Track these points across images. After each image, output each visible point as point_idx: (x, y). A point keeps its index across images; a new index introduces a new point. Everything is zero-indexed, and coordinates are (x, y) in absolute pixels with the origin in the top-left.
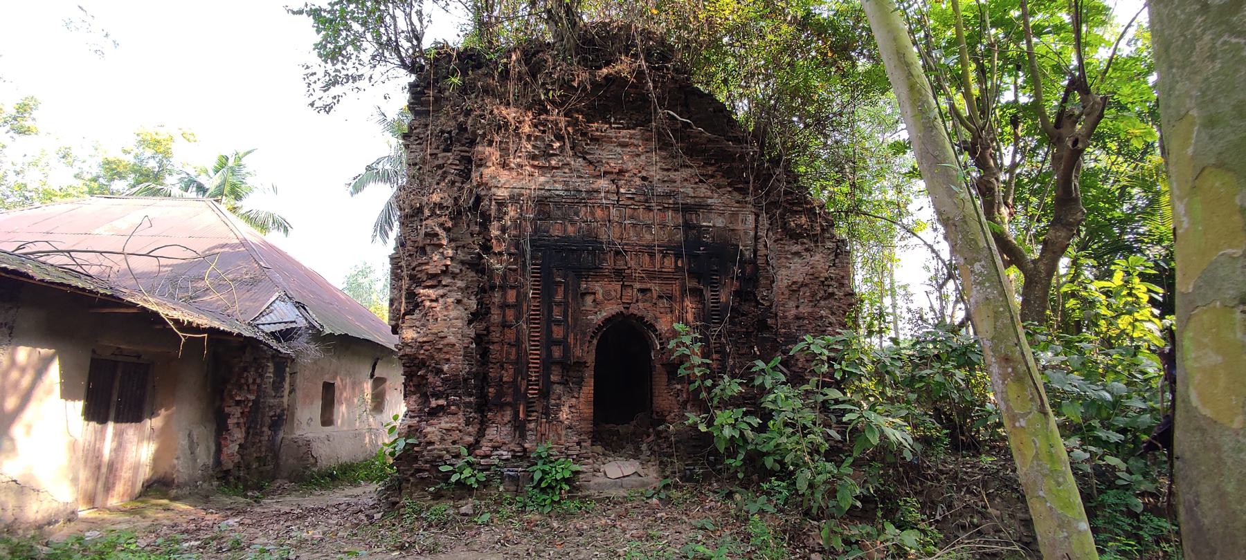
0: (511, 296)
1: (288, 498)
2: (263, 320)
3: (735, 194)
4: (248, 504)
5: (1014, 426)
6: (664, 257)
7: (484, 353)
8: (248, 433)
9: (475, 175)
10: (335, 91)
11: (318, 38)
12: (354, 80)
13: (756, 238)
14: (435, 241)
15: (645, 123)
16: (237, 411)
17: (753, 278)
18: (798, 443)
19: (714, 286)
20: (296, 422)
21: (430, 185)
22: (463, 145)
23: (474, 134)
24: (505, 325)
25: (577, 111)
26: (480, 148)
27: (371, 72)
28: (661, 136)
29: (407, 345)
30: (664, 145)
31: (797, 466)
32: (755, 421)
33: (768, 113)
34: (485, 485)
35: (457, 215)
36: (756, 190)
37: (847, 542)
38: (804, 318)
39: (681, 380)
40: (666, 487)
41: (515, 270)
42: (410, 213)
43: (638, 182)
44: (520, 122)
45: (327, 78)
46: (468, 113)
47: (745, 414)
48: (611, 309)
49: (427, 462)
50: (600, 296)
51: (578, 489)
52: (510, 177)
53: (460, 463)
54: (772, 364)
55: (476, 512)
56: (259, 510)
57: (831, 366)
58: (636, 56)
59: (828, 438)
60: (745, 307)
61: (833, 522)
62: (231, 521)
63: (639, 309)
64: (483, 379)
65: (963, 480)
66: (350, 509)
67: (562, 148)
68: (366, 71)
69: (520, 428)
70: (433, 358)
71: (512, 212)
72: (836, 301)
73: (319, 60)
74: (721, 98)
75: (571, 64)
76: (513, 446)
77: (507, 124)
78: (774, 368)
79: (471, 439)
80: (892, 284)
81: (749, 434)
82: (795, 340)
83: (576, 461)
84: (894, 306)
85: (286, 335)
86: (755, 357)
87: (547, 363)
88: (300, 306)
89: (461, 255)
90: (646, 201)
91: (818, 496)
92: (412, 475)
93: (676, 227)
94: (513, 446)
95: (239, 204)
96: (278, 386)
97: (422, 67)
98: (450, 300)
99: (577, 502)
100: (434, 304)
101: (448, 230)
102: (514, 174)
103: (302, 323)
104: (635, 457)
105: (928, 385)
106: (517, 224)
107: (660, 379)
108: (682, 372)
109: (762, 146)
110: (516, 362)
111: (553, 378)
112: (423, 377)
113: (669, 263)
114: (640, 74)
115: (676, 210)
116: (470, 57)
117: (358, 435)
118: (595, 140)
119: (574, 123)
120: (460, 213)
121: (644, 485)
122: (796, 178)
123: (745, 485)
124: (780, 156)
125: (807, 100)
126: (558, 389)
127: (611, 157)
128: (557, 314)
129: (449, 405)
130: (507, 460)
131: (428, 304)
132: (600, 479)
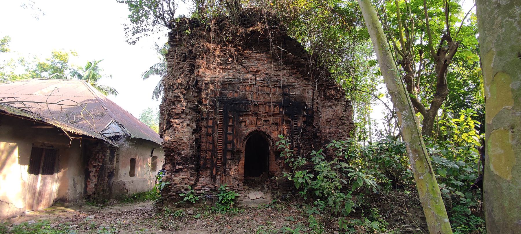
0: (211, 123)
1: (115, 207)
2: (105, 132)
3: (305, 81)
4: (98, 209)
5: (419, 179)
6: (275, 107)
7: (199, 147)
8: (98, 179)
9: (196, 72)
10: (137, 35)
11: (130, 13)
12: (145, 31)
13: (313, 99)
14: (179, 99)
15: (267, 51)
16: (94, 170)
17: (311, 116)
18: (329, 185)
19: (296, 119)
20: (119, 175)
21: (177, 75)
22: (191, 59)
23: (196, 54)
24: (208, 135)
25: (239, 46)
26: (198, 60)
27: (152, 28)
28: (274, 56)
29: (166, 143)
30: (275, 60)
31: (329, 195)
32: (312, 176)
33: (319, 48)
34: (199, 202)
35: (188, 88)
36: (313, 79)
37: (349, 226)
38: (332, 133)
39: (281, 158)
40: (274, 203)
41: (212, 112)
42: (168, 87)
43: (264, 75)
44: (215, 50)
45: (134, 30)
46: (193, 46)
47: (307, 173)
48: (252, 129)
49: (174, 192)
50: (248, 123)
51: (237, 204)
52: (210, 73)
53: (188, 192)
54: (319, 152)
55: (195, 213)
56: (103, 212)
57: (343, 153)
58: (264, 23)
59: (342, 183)
60: (308, 128)
61: (343, 218)
62: (91, 217)
63: (264, 128)
64: (198, 157)
65: (397, 201)
66: (142, 212)
67: (232, 61)
68: (150, 27)
69: (213, 178)
70: (177, 148)
71: (211, 87)
72: (346, 126)
73: (131, 23)
74: (299, 41)
75: (237, 26)
76: (210, 186)
77: (209, 50)
78: (320, 154)
79: (193, 183)
80: (369, 119)
81: (309, 181)
82: (329, 142)
83: (237, 192)
84: (370, 129)
85: (115, 138)
86: (312, 149)
87: (225, 151)
88: (121, 126)
89: (189, 105)
90: (267, 84)
91: (337, 207)
92: (168, 198)
93: (280, 94)
94: (210, 186)
95: (96, 83)
96: (111, 160)
97: (174, 26)
98: (185, 124)
99: (237, 209)
100: (178, 126)
101: (184, 95)
102: (212, 71)
103: (122, 133)
104: (262, 191)
105: (383, 161)
106: (213, 92)
107: (273, 158)
108: (281, 155)
109: (316, 61)
110: (212, 150)
111: (228, 157)
112: (173, 156)
113: (277, 110)
114: (265, 30)
115: (280, 87)
116: (194, 22)
117: (145, 181)
118: (246, 58)
119: (238, 50)
120: (189, 88)
121: (265, 202)
122: (330, 74)
123: (307, 202)
124: (323, 65)
125: (335, 42)
126: (230, 162)
127: (253, 65)
128: (229, 130)
129: (183, 168)
130: (208, 191)
131: (175, 125)
132: (247, 200)
